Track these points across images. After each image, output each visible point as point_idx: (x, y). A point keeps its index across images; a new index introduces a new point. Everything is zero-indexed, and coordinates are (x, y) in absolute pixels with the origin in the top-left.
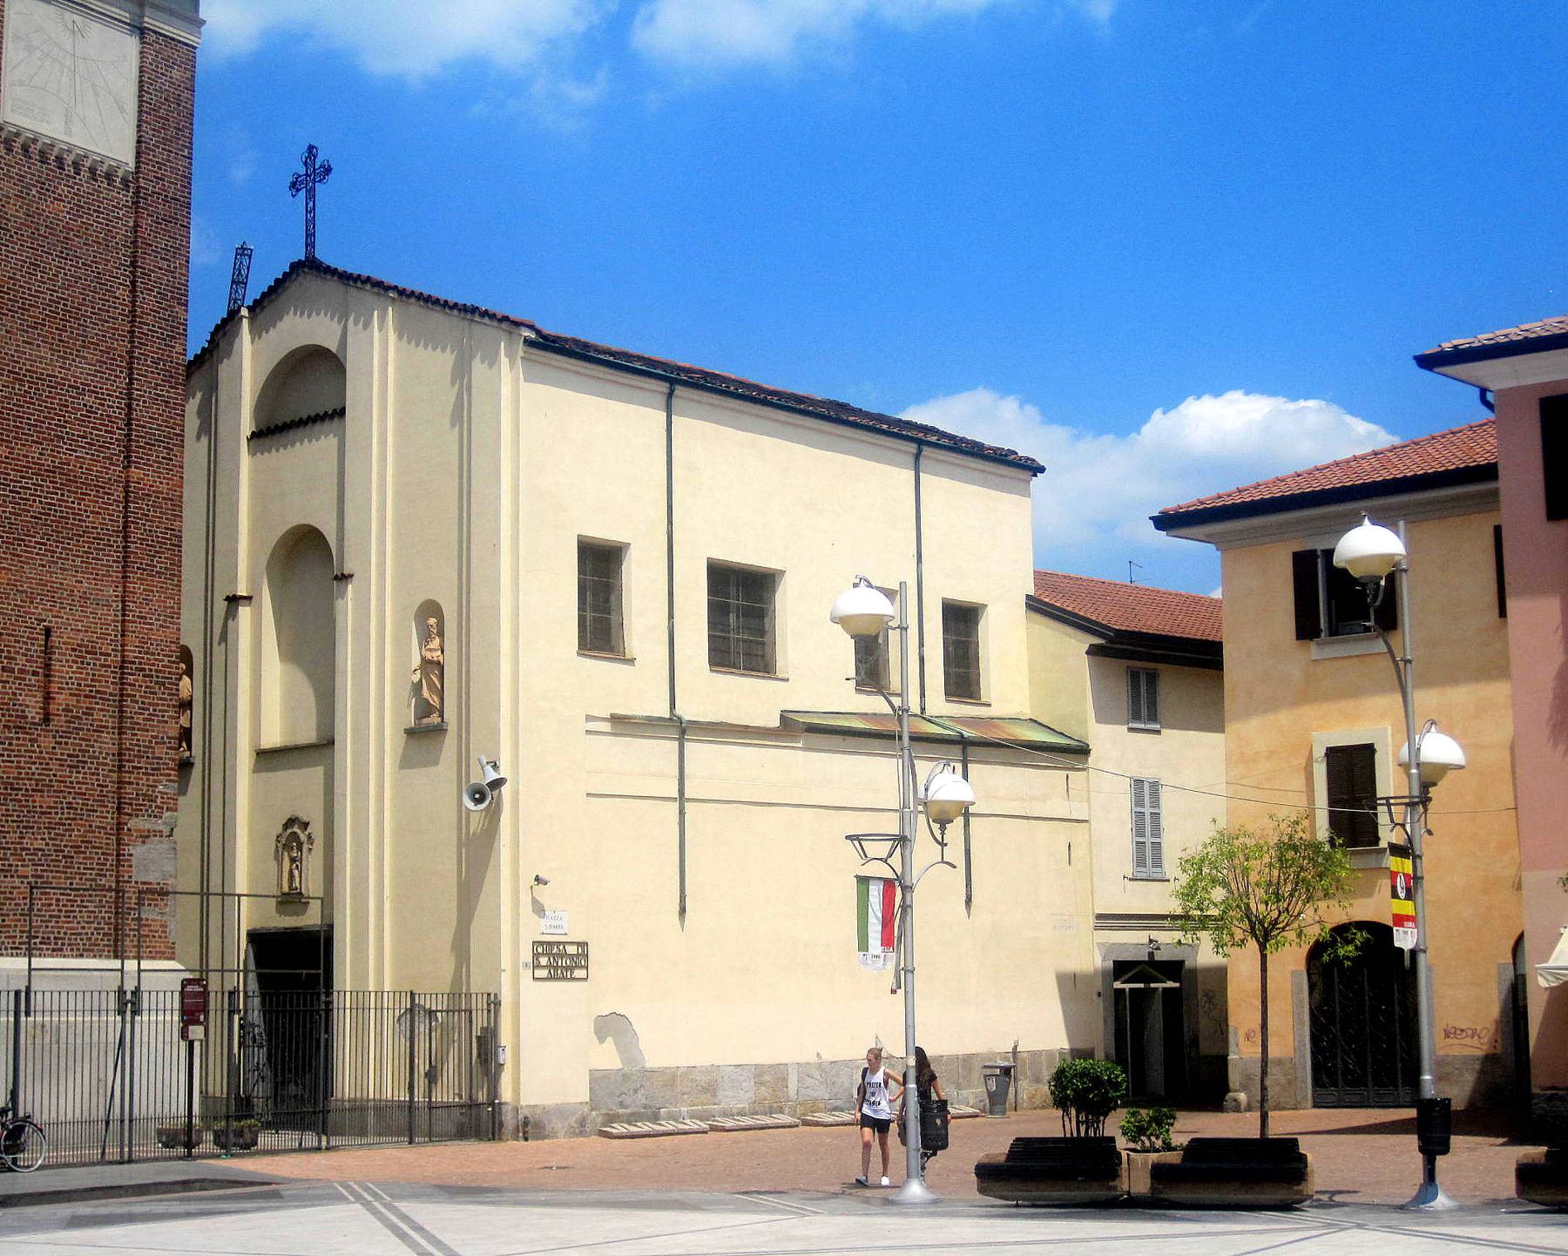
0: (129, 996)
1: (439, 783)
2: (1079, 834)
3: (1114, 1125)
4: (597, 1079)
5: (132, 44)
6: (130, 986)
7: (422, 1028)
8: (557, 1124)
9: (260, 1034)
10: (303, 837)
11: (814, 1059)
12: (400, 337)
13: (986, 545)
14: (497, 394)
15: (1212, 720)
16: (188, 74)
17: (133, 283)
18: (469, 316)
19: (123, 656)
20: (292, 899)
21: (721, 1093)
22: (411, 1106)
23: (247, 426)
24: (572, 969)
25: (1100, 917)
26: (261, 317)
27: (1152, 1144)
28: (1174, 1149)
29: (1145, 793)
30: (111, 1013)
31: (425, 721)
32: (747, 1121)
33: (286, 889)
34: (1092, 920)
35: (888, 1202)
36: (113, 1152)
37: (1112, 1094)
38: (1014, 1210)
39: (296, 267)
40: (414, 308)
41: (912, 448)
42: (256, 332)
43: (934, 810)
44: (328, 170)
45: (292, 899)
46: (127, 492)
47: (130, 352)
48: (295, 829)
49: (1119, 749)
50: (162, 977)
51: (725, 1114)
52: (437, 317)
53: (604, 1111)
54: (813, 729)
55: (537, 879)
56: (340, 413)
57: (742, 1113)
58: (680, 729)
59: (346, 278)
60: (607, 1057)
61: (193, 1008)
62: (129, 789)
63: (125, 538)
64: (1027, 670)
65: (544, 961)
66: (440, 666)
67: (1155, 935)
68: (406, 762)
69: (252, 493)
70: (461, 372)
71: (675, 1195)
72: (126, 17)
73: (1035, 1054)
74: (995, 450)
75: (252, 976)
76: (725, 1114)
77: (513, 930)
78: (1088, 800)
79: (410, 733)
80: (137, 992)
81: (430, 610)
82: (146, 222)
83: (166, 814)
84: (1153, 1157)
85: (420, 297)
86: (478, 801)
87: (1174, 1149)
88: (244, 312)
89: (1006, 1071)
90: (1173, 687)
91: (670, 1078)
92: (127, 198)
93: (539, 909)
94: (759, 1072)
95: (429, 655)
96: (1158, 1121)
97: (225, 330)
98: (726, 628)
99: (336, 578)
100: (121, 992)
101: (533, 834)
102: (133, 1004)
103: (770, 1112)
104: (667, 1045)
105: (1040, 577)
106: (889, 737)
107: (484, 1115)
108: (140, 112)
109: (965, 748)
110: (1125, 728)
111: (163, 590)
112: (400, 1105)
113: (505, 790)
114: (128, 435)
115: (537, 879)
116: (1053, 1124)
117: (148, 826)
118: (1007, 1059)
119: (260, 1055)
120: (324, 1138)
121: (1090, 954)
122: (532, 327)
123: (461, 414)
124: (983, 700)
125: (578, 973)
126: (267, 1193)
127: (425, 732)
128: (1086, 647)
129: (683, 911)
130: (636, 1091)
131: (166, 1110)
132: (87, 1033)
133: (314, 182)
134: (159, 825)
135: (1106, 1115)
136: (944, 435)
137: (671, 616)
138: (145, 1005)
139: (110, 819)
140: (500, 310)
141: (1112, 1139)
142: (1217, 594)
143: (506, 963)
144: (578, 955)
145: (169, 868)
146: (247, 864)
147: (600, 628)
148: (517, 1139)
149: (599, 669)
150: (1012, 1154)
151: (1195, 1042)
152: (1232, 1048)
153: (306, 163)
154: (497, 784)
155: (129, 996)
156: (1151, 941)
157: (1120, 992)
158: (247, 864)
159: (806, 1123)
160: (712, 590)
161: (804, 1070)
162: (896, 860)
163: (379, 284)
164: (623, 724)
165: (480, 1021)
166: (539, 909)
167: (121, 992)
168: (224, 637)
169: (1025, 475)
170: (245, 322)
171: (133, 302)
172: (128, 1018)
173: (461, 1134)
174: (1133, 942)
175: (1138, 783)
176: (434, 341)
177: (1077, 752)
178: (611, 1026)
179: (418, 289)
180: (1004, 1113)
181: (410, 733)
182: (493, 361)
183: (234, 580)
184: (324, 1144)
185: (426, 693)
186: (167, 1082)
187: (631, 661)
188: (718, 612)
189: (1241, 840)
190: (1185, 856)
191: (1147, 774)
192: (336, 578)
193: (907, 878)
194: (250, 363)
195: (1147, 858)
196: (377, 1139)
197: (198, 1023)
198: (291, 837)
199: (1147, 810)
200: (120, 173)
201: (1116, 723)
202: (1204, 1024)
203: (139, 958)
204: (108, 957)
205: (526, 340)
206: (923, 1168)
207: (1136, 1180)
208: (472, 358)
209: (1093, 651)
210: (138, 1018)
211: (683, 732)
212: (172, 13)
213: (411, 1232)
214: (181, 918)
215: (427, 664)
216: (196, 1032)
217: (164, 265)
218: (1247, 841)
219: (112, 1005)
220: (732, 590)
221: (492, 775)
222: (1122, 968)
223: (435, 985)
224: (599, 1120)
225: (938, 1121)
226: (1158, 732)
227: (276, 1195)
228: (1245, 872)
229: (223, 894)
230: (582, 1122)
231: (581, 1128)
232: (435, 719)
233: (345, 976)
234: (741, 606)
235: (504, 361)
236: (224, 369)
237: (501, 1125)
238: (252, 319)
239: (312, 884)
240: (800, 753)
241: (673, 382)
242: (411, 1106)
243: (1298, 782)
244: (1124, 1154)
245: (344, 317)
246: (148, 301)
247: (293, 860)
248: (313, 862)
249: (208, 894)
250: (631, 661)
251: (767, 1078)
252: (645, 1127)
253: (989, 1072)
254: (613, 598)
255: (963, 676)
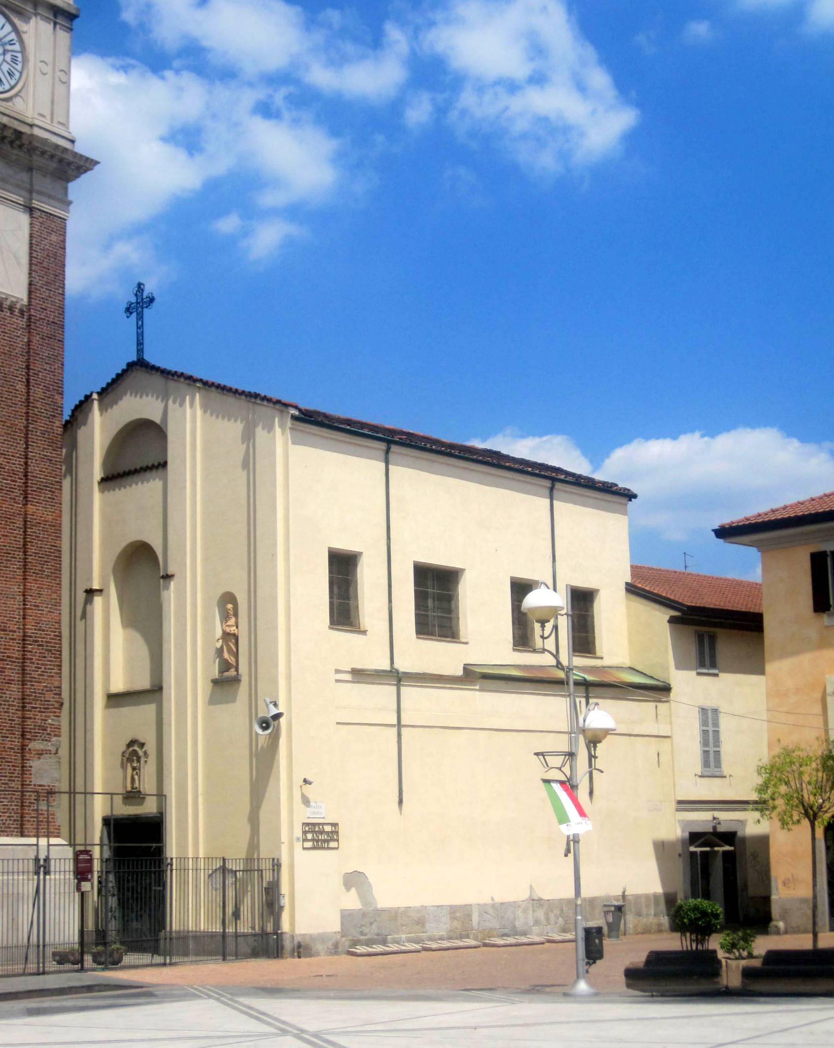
0: (42, 862)
1: (236, 714)
2: (665, 745)
3: (715, 942)
4: (346, 916)
5: (24, 219)
6: (42, 856)
7: (230, 880)
8: (319, 947)
9: (113, 887)
10: (141, 753)
11: (490, 902)
12: (205, 412)
13: (596, 549)
14: (273, 454)
15: (754, 664)
16: (61, 238)
17: (28, 381)
18: (253, 400)
19: (24, 632)
20: (133, 796)
21: (427, 925)
22: (224, 935)
23: (98, 473)
24: (328, 841)
25: (680, 802)
26: (107, 400)
27: (740, 955)
28: (756, 957)
29: (709, 717)
30: (31, 874)
31: (226, 674)
32: (446, 944)
33: (129, 789)
34: (674, 805)
35: (565, 995)
36: (32, 967)
37: (713, 921)
38: (650, 999)
39: (131, 366)
40: (214, 394)
41: (548, 483)
42: (103, 409)
43: (589, 734)
44: (152, 300)
45: (133, 796)
46: (25, 521)
47: (26, 427)
48: (136, 748)
49: (691, 688)
50: (59, 850)
51: (431, 939)
52: (230, 400)
53: (350, 938)
54: (485, 677)
55: (305, 781)
56: (164, 465)
57: (442, 939)
58: (397, 678)
59: (166, 373)
60: (352, 901)
61: (82, 872)
62: (29, 722)
63: (25, 553)
64: (628, 634)
65: (309, 836)
66: (236, 637)
67: (717, 814)
68: (213, 701)
69: (102, 522)
70: (248, 436)
71: (421, 992)
72: (21, 200)
73: (637, 897)
74: (604, 483)
75: (106, 848)
76: (431, 939)
77: (288, 816)
78: (671, 723)
79: (215, 682)
80: (47, 860)
81: (228, 598)
82: (36, 339)
83: (54, 739)
84: (743, 963)
85: (218, 387)
86: (265, 729)
87: (756, 957)
88: (95, 396)
89: (619, 909)
90: (727, 645)
91: (394, 915)
92: (22, 322)
93: (306, 801)
94: (453, 910)
95: (228, 630)
96: (746, 939)
97: (83, 406)
98: (426, 608)
99: (163, 577)
100: (37, 860)
101: (302, 750)
102: (45, 867)
103: (461, 937)
104: (390, 894)
105: (636, 570)
106: (560, 682)
107: (271, 942)
108: (31, 264)
109: (595, 687)
110: (694, 673)
111: (50, 588)
112: (212, 936)
113: (282, 720)
114: (26, 483)
115: (305, 781)
116: (674, 943)
117: (42, 747)
118: (618, 900)
119: (113, 902)
120: (168, 958)
121: (673, 829)
122: (296, 407)
123: (248, 463)
124: (598, 654)
125: (333, 844)
126: (141, 994)
127: (225, 682)
128: (667, 617)
129: (401, 802)
130: (371, 924)
131: (57, 939)
132: (21, 886)
133: (142, 308)
134: (49, 746)
135: (709, 935)
136: (567, 473)
137: (390, 601)
138: (52, 869)
139: (17, 743)
140: (275, 396)
141: (715, 952)
142: (759, 580)
143: (284, 837)
144: (332, 832)
145: (56, 775)
146: (102, 773)
147: (343, 612)
148: (293, 957)
149: (343, 637)
150: (648, 962)
151: (745, 887)
152: (774, 891)
153: (136, 295)
154: (277, 717)
155: (42, 862)
156: (714, 818)
157: (693, 854)
158: (102, 773)
159: (485, 945)
160: (417, 583)
161: (483, 909)
162: (567, 769)
163: (190, 378)
164: (359, 675)
165: (268, 876)
166: (306, 801)
167: (37, 860)
168: (84, 616)
169: (624, 500)
170: (96, 404)
171: (28, 393)
172: (42, 877)
173: (255, 953)
174: (702, 819)
175: (703, 711)
176: (228, 415)
177: (662, 690)
178: (354, 880)
179: (247, 389)
180: (618, 937)
181: (215, 682)
182: (270, 429)
183: (90, 579)
184: (168, 961)
185: (226, 655)
186: (57, 921)
187: (364, 632)
188: (421, 597)
189: (797, 753)
190: (761, 765)
191: (709, 704)
192: (163, 577)
193: (574, 780)
194: (99, 431)
195: (711, 763)
196: (194, 958)
197: (87, 880)
198: (133, 753)
199: (711, 729)
200: (18, 306)
201: (690, 669)
202: (752, 875)
203: (48, 836)
204: (16, 836)
205: (294, 418)
206: (587, 972)
207: (731, 977)
208: (255, 426)
209: (672, 621)
210: (48, 877)
211: (399, 680)
212: (50, 197)
213: (261, 1016)
214: (60, 808)
215: (226, 636)
216: (86, 886)
217: (47, 367)
218: (800, 753)
219: (32, 868)
220: (430, 583)
221: (274, 711)
222: (695, 837)
223: (236, 853)
224: (347, 943)
225: (597, 941)
226: (716, 675)
227: (150, 995)
228: (801, 774)
229: (85, 793)
230: (336, 945)
231: (335, 950)
232: (232, 673)
233: (172, 850)
234: (437, 593)
235: (278, 430)
236: (81, 433)
237: (283, 947)
238: (100, 401)
239: (148, 784)
240: (478, 693)
241: (389, 442)
242: (224, 935)
243: (817, 709)
244: (723, 961)
245: (165, 397)
246: (37, 392)
247: (134, 769)
248: (149, 770)
249: (75, 793)
250: (364, 632)
251: (458, 914)
252: (379, 948)
253: (606, 909)
254: (351, 589)
255: (584, 639)
